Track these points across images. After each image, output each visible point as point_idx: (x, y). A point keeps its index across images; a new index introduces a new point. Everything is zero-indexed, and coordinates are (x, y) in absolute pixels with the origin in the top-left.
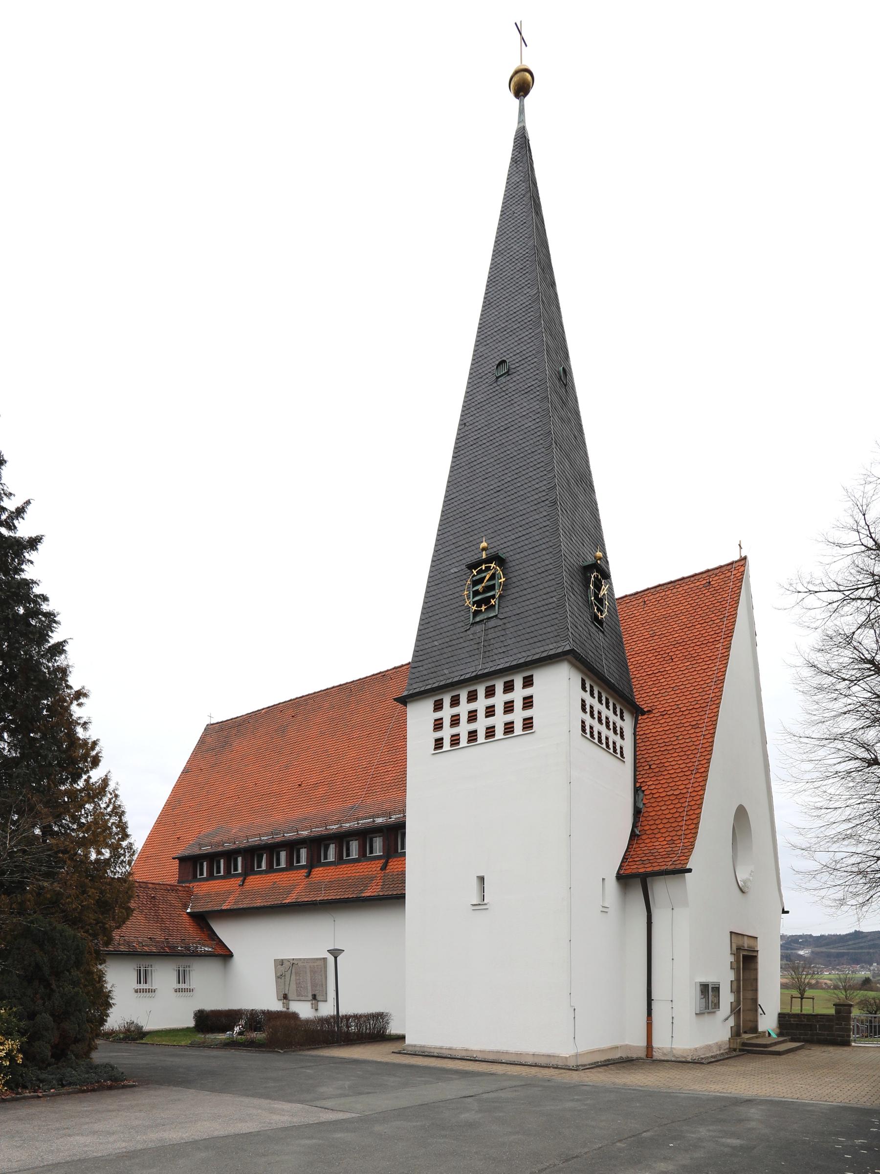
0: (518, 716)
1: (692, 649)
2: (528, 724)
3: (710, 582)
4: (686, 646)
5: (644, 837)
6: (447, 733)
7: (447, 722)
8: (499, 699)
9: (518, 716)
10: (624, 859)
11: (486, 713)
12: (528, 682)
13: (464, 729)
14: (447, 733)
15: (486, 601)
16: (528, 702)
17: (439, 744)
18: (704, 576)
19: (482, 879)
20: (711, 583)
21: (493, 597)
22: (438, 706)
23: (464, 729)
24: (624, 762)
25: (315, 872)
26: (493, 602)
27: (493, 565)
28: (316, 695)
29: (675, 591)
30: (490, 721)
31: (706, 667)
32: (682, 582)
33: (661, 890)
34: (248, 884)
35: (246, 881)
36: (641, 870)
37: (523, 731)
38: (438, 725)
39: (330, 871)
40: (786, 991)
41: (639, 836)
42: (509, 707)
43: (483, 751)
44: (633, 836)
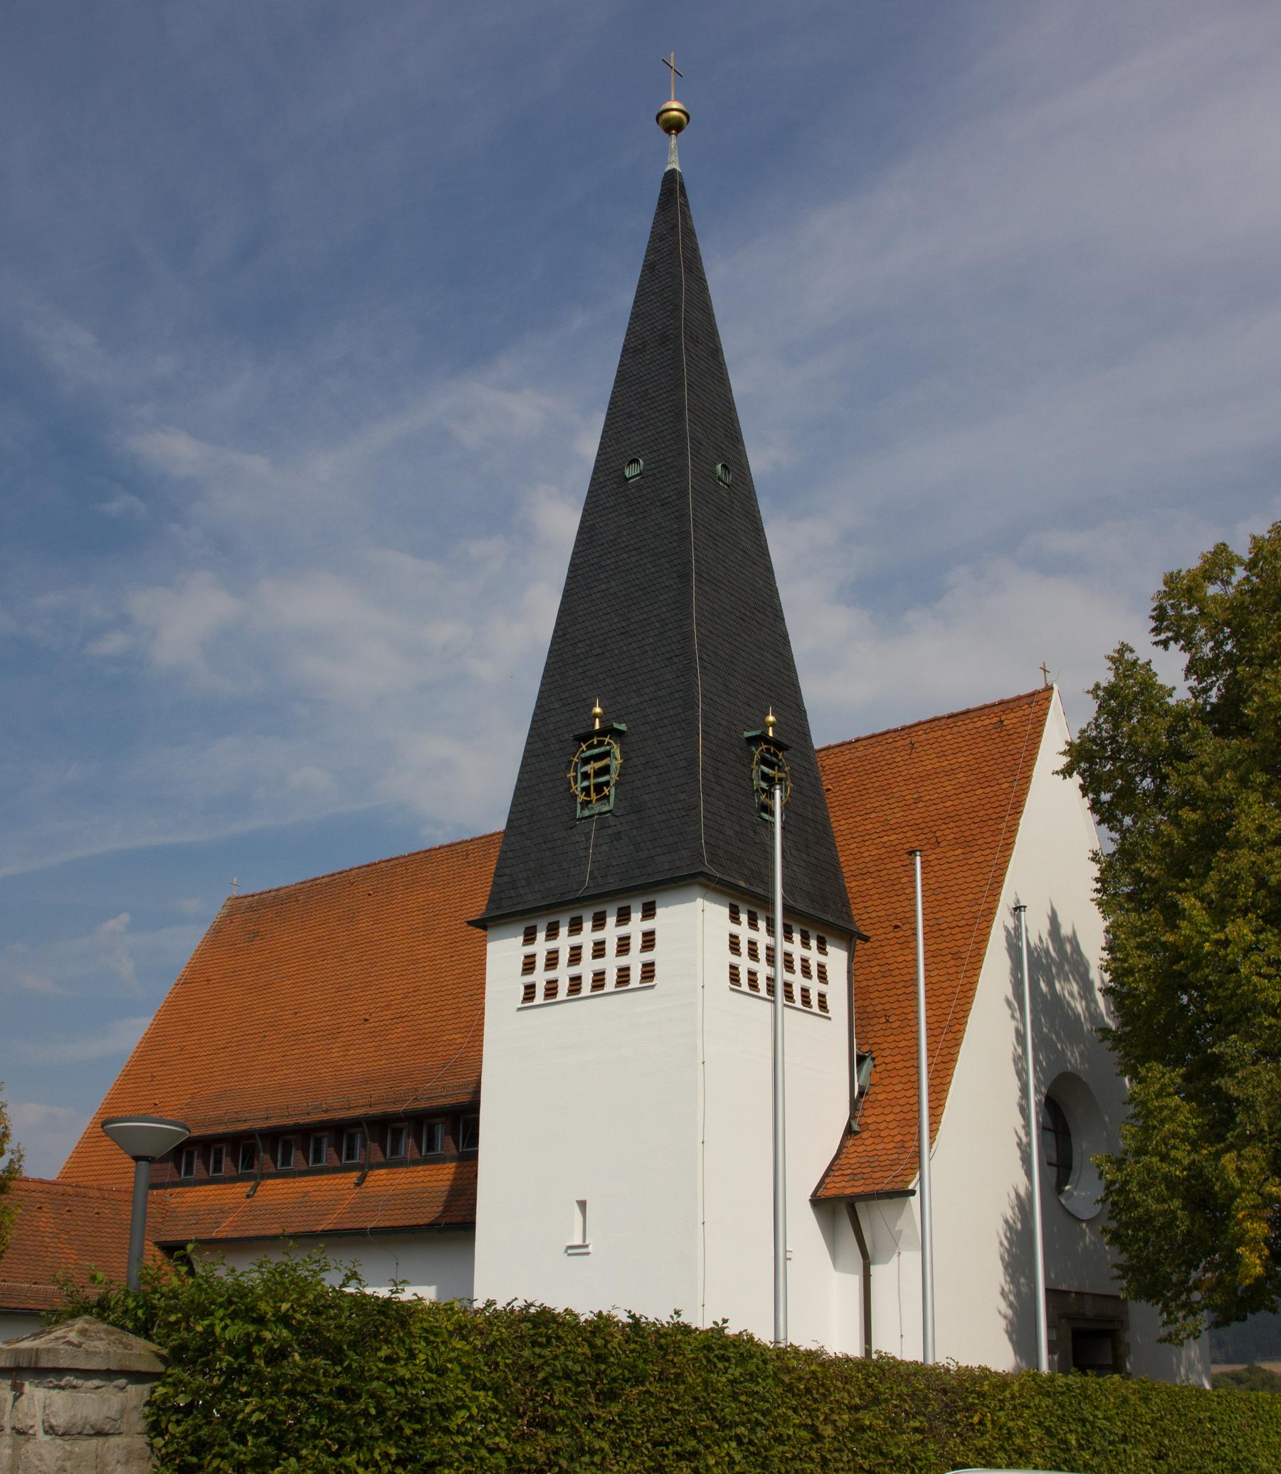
0: (635, 960)
1: (967, 827)
2: (648, 971)
3: (1002, 722)
4: (960, 823)
5: (865, 1135)
6: (540, 977)
7: (541, 962)
8: (611, 932)
9: (635, 960)
10: (830, 1169)
11: (594, 951)
12: (649, 912)
13: (563, 974)
14: (540, 977)
15: (599, 788)
16: (649, 941)
17: (530, 991)
18: (996, 709)
19: (582, 1205)
20: (1005, 723)
21: (607, 784)
22: (530, 937)
23: (563, 974)
24: (829, 1019)
25: (372, 1178)
26: (606, 791)
27: (607, 740)
28: (412, 858)
29: (956, 730)
30: (599, 964)
31: (982, 859)
32: (966, 716)
33: (875, 1219)
34: (262, 1193)
35: (259, 1188)
36: (848, 1191)
37: (641, 983)
38: (529, 966)
39: (397, 1175)
40: (34, 1354)
41: (856, 1133)
42: (624, 946)
43: (589, 1009)
44: (849, 1131)
